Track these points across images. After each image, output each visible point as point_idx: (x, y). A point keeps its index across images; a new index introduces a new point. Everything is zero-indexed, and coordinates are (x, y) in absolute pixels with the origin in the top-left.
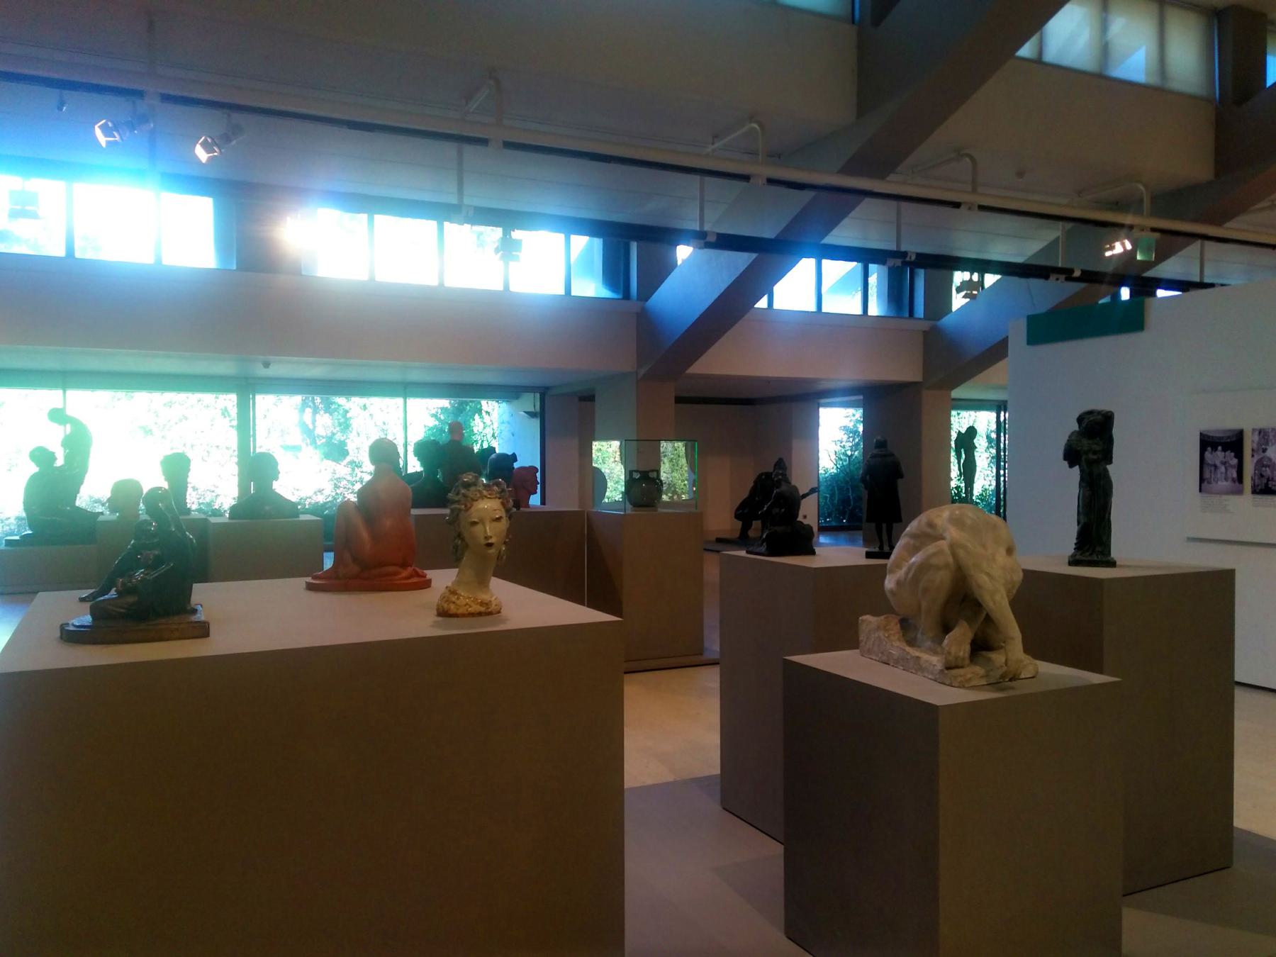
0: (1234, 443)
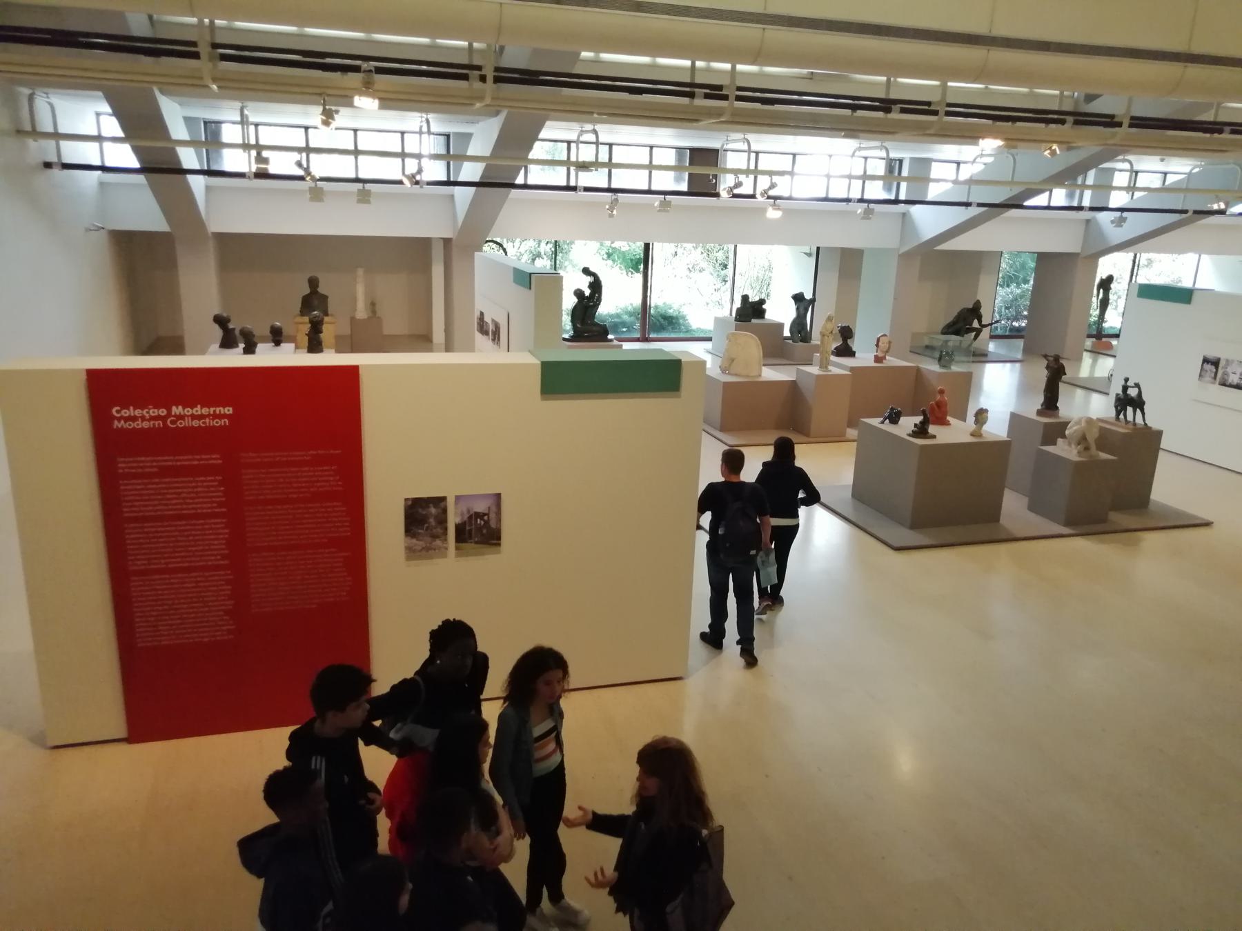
0: (1216, 363)
